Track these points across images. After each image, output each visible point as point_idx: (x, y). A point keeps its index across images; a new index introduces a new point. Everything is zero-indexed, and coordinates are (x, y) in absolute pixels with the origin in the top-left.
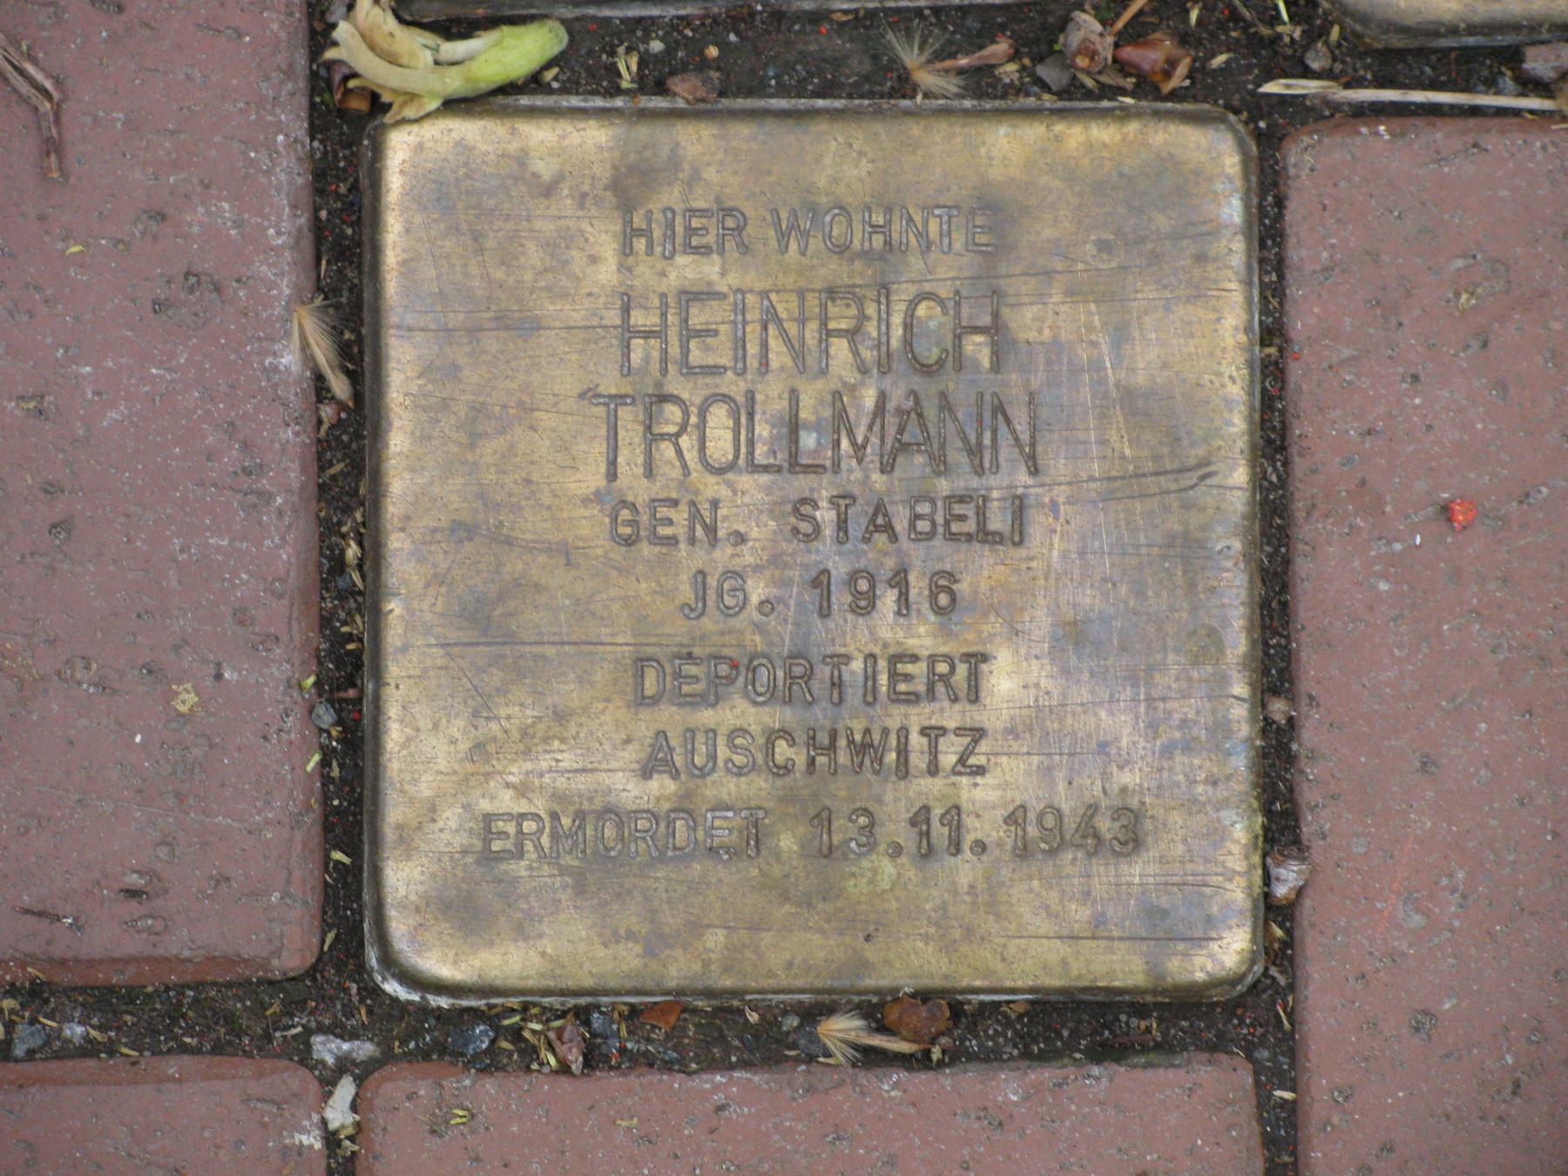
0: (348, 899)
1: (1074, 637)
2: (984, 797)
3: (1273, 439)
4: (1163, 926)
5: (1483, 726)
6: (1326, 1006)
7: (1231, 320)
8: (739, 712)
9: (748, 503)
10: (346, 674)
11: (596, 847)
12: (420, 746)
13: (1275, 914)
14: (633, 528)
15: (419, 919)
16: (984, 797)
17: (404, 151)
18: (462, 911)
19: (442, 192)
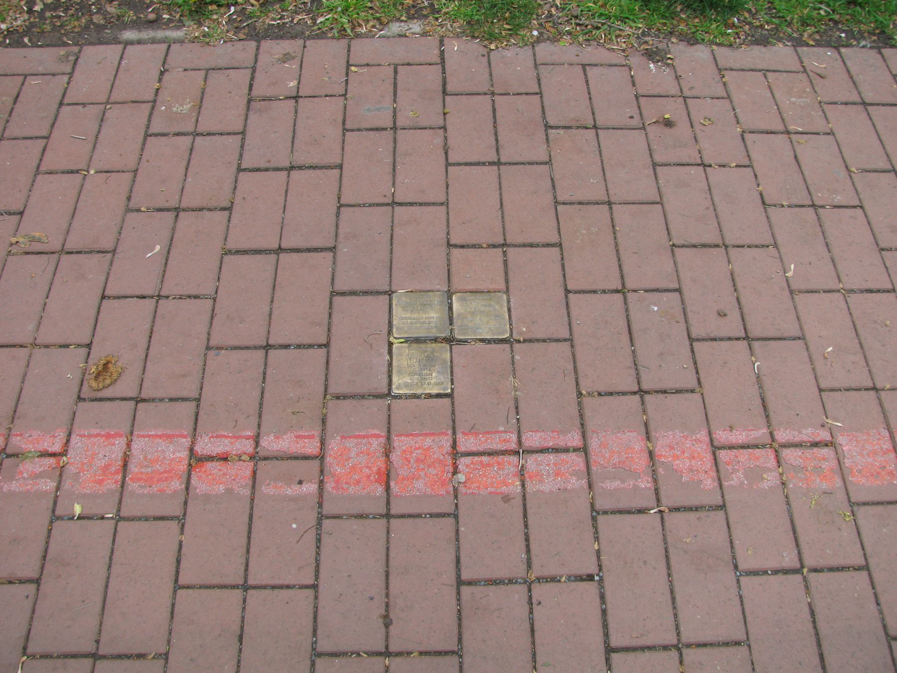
0: (390, 389)
1: (438, 372)
2: (432, 381)
3: (451, 362)
4: (445, 389)
5: (656, 309)
6: (455, 394)
7: (449, 355)
8: (416, 377)
9: (417, 365)
10: (390, 377)
11: (407, 385)
12: (395, 379)
13: (452, 389)
14: (409, 366)
15: (625, 8)
16: (432, 381)
17: (394, 346)
18: (398, 388)
19: (397, 348)
